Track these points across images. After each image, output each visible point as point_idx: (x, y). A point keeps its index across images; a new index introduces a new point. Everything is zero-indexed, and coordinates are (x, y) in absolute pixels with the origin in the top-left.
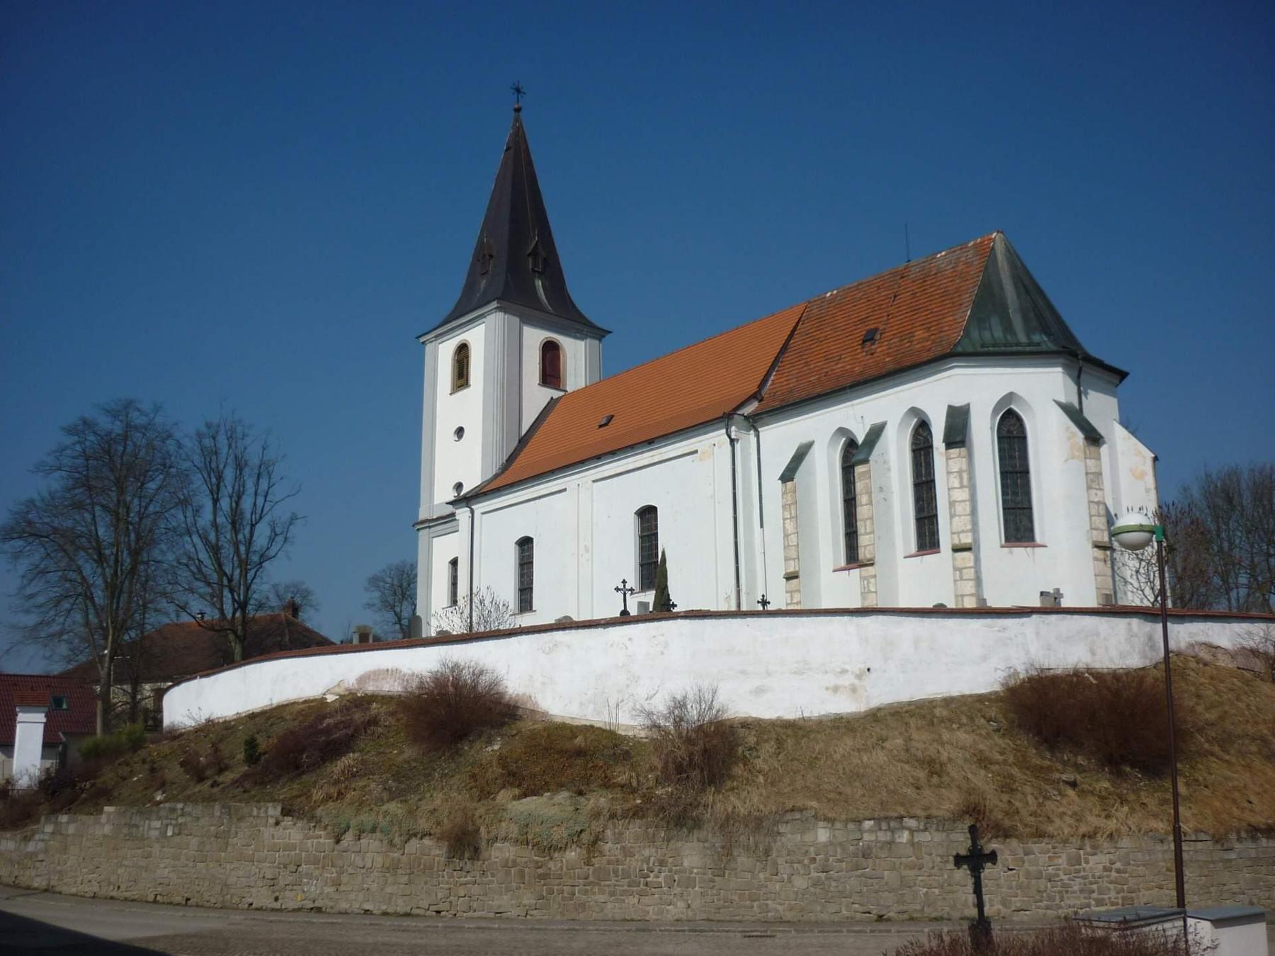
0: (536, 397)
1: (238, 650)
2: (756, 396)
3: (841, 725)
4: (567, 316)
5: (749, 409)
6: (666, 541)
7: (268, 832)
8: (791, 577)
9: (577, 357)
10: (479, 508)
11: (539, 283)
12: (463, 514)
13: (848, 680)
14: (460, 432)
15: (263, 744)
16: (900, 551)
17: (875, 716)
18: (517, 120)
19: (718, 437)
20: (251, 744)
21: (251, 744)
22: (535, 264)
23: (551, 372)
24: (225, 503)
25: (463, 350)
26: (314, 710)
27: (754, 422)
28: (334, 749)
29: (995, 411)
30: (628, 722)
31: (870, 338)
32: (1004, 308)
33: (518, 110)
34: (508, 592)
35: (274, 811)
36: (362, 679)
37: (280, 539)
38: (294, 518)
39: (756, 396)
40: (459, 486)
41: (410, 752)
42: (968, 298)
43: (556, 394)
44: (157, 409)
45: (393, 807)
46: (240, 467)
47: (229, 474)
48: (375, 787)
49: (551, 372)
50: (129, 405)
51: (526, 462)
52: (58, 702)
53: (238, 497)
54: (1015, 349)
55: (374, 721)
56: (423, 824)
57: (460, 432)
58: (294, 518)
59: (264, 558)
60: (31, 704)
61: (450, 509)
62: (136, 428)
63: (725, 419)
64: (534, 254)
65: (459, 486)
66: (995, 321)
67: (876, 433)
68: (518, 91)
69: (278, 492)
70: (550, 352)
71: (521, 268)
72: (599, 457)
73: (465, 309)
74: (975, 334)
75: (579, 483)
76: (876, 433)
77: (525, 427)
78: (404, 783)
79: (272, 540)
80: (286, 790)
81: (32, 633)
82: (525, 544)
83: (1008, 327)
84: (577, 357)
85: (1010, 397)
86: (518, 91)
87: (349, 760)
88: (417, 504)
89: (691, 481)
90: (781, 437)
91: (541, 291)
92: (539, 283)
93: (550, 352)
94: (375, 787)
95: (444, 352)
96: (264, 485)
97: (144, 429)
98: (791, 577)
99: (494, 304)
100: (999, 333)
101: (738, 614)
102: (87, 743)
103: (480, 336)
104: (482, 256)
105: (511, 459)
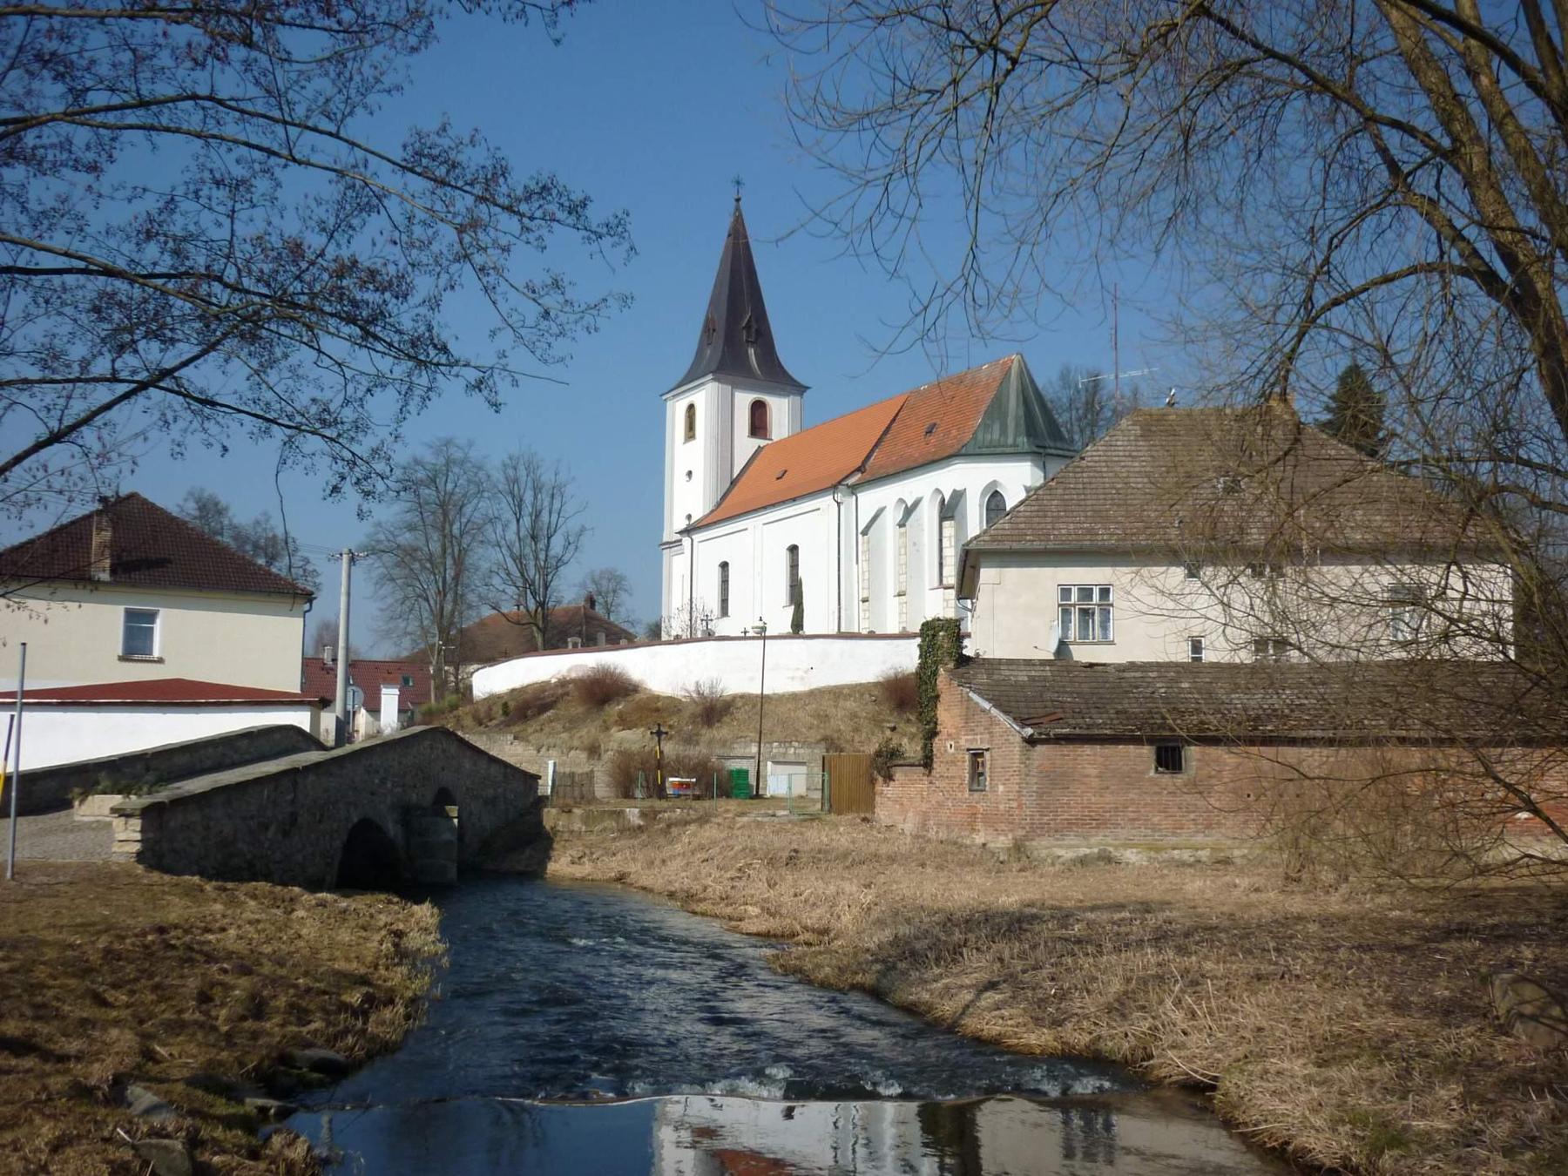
0: (746, 446)
1: (539, 639)
2: (858, 470)
3: (794, 697)
4: (778, 378)
5: (851, 481)
6: (801, 573)
7: (507, 747)
8: (865, 601)
9: (780, 409)
10: (697, 537)
11: (751, 351)
12: (686, 541)
13: (801, 673)
14: (690, 474)
15: (512, 704)
16: (927, 587)
17: (812, 693)
18: (738, 209)
19: (826, 502)
20: (505, 705)
21: (505, 705)
22: (749, 335)
23: (759, 422)
24: (526, 521)
25: (691, 407)
26: (543, 687)
27: (854, 489)
28: (544, 708)
29: (983, 494)
30: (679, 694)
31: (929, 432)
32: (1005, 415)
33: (738, 200)
34: (714, 605)
35: (510, 737)
36: (569, 670)
37: (572, 547)
38: (583, 530)
39: (858, 470)
40: (689, 517)
41: (581, 709)
42: (984, 408)
43: (762, 443)
44: (471, 444)
45: (565, 735)
46: (537, 489)
47: (528, 497)
48: (559, 727)
49: (759, 422)
50: (448, 443)
51: (735, 501)
52: (406, 681)
53: (537, 515)
54: (999, 450)
55: (567, 694)
56: (576, 743)
57: (690, 474)
58: (583, 530)
59: (560, 562)
60: (390, 683)
61: (678, 537)
62: (454, 462)
63: (834, 488)
64: (748, 327)
65: (689, 517)
66: (997, 427)
67: (917, 503)
68: (738, 183)
69: (569, 509)
70: (758, 409)
71: (740, 341)
72: (765, 508)
73: (691, 377)
74: (980, 436)
75: (754, 523)
76: (917, 503)
77: (736, 472)
78: (572, 724)
79: (566, 548)
80: (516, 729)
81: (387, 634)
82: (793, 549)
83: (1004, 431)
84: (780, 409)
85: (994, 483)
86: (738, 183)
87: (549, 713)
88: (662, 529)
89: (814, 524)
90: (870, 499)
91: (753, 358)
92: (751, 351)
93: (758, 409)
94: (559, 727)
95: (677, 409)
96: (557, 505)
97: (462, 463)
98: (865, 601)
99: (710, 376)
100: (996, 436)
101: (745, 638)
102: (424, 707)
103: (705, 396)
104: (709, 329)
105: (719, 505)
